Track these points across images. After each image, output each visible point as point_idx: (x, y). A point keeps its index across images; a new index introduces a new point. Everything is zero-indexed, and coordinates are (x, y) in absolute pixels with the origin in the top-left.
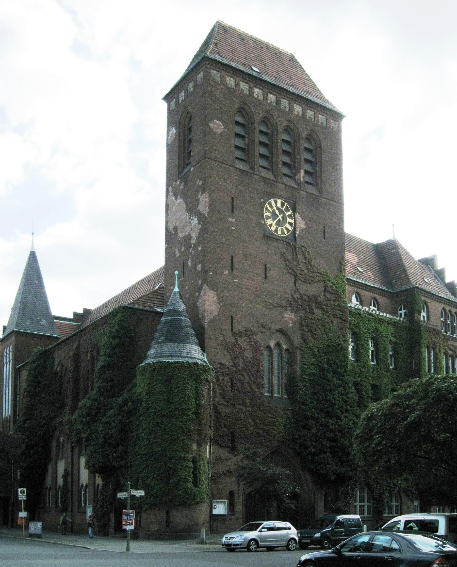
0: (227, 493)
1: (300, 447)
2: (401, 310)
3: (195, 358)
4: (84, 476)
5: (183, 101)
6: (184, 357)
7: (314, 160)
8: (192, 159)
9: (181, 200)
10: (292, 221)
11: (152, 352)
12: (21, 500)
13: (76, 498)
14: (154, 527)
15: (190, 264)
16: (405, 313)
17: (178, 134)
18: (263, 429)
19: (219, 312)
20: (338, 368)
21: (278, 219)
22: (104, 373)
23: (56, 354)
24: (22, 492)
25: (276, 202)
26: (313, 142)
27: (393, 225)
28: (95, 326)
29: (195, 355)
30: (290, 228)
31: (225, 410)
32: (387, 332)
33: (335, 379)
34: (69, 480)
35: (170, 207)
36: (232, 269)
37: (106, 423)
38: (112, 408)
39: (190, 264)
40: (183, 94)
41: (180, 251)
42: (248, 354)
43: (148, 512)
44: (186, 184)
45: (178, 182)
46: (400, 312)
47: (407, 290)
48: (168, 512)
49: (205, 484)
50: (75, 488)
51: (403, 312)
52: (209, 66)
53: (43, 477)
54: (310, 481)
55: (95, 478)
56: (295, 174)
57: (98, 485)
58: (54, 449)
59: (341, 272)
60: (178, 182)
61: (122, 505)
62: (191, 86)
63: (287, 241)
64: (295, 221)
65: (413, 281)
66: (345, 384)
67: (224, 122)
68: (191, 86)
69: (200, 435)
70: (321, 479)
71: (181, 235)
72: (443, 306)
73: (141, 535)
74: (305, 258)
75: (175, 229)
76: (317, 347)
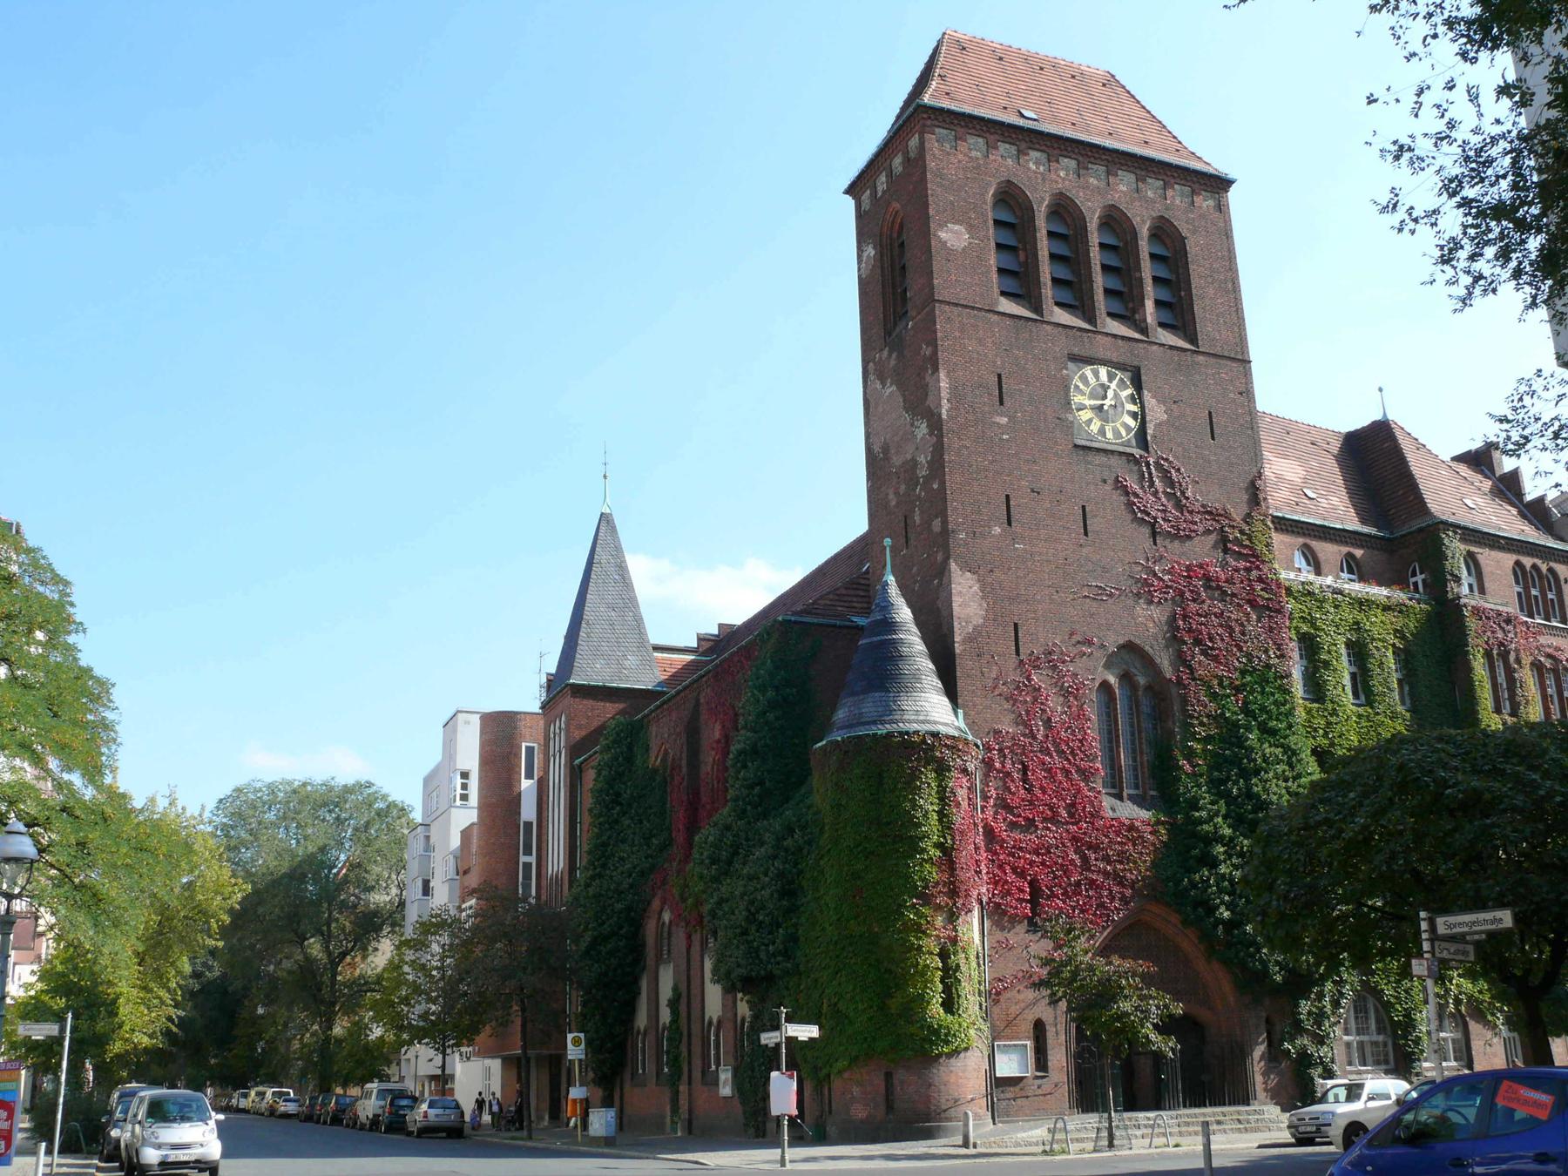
0: (1027, 1026)
1: (1195, 908)
2: (1414, 574)
3: (936, 723)
4: (714, 999)
5: (884, 192)
6: (910, 722)
7: (1173, 277)
8: (909, 305)
9: (894, 388)
10: (1134, 408)
11: (841, 715)
12: (778, 1119)
13: (697, 1049)
14: (859, 1112)
15: (917, 518)
16: (1424, 581)
17: (881, 255)
18: (1106, 874)
19: (986, 619)
20: (1270, 718)
21: (1101, 406)
22: (745, 767)
23: (653, 729)
24: (576, 1042)
25: (1096, 374)
26: (1168, 241)
27: (1381, 390)
28: (747, 652)
29: (935, 716)
30: (1132, 423)
31: (1011, 837)
32: (1380, 628)
33: (1266, 745)
34: (683, 1008)
35: (872, 404)
36: (1009, 524)
37: (751, 878)
38: (762, 844)
39: (917, 518)
40: (883, 178)
41: (896, 493)
42: (1055, 704)
43: (846, 1075)
44: (901, 356)
45: (886, 353)
46: (1412, 580)
47: (1421, 530)
48: (888, 1076)
49: (971, 1002)
50: (696, 1028)
51: (1419, 578)
52: (929, 122)
53: (630, 1008)
54: (1227, 987)
55: (735, 1002)
56: (1134, 311)
57: (743, 1020)
58: (650, 941)
59: (1258, 504)
60: (886, 353)
61: (770, 1058)
62: (897, 161)
63: (1128, 450)
64: (1143, 407)
65: (1433, 506)
66: (1291, 753)
67: (971, 228)
68: (897, 161)
69: (953, 893)
70: (1253, 982)
71: (897, 460)
72: (1514, 557)
73: (832, 1130)
74: (1171, 484)
75: (886, 449)
76: (1216, 676)
